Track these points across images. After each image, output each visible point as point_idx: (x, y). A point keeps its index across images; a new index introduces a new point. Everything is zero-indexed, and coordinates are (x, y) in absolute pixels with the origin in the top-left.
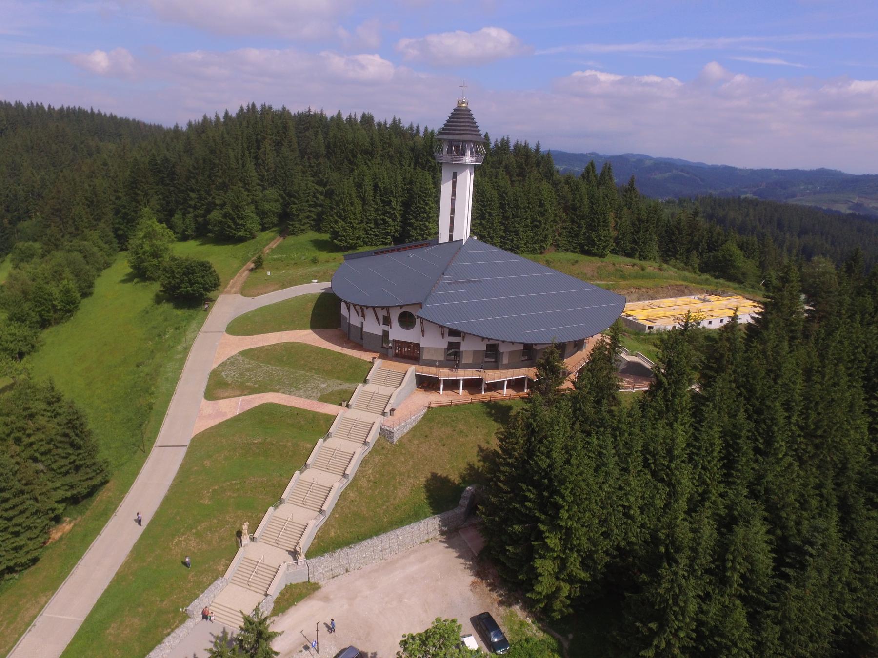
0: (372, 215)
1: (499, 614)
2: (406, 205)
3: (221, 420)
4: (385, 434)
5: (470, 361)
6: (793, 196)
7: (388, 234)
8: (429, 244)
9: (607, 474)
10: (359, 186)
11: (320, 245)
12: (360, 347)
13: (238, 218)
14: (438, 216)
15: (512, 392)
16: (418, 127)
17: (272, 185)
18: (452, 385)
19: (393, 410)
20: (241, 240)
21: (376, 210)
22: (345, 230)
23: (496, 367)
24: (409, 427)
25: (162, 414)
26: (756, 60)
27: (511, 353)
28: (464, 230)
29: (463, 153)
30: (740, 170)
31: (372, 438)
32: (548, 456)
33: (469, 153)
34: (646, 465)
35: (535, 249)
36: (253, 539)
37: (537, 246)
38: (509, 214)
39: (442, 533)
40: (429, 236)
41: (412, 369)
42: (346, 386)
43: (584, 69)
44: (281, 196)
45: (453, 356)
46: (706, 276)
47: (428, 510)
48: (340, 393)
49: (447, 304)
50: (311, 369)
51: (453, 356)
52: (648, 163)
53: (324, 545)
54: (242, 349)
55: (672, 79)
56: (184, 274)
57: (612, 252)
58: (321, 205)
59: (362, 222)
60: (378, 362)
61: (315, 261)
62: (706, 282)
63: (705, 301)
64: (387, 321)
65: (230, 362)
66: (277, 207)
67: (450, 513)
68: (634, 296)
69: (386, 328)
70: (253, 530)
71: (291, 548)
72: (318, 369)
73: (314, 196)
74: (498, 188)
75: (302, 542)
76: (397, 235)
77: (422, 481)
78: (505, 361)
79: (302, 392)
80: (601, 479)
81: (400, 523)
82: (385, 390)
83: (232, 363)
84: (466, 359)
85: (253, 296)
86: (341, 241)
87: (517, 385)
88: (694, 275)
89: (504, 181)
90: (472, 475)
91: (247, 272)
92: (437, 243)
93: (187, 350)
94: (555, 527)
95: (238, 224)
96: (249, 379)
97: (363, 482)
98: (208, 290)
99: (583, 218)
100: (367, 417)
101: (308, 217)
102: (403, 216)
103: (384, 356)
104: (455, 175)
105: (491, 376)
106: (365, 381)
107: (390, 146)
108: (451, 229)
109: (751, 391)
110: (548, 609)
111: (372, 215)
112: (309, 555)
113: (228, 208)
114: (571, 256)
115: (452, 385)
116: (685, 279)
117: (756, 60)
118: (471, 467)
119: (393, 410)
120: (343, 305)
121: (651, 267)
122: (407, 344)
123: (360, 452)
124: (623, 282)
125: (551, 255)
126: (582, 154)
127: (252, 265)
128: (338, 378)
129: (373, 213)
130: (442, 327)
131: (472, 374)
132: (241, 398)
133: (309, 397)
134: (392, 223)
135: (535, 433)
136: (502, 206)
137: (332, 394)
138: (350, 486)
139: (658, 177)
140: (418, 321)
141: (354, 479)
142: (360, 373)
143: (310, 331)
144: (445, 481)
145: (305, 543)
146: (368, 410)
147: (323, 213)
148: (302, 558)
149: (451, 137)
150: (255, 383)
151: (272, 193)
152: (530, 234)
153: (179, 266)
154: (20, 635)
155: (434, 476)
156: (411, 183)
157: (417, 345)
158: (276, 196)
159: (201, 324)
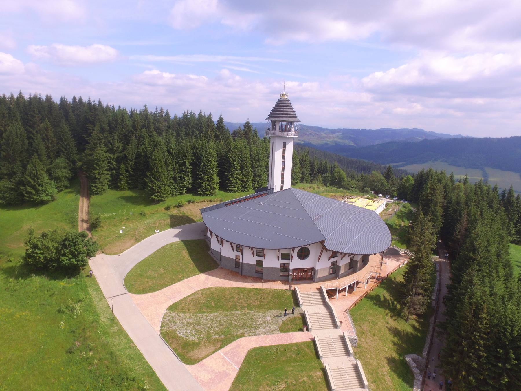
16: (113, 106)
20: (43, 203)
30: (235, 124)
40: (263, 189)
43: (150, 69)
50: (242, 308)
51: (335, 273)
54: (171, 303)
55: (203, 77)
58: (114, 169)
61: (142, 214)
76: (190, 186)
85: (118, 253)
86: (157, 196)
92: (273, 193)
93: (113, 319)
95: (39, 190)
122: (303, 270)
128: (270, 309)
132: (221, 352)
134: (187, 178)
151: (61, 161)
158: (63, 165)
159: (98, 290)
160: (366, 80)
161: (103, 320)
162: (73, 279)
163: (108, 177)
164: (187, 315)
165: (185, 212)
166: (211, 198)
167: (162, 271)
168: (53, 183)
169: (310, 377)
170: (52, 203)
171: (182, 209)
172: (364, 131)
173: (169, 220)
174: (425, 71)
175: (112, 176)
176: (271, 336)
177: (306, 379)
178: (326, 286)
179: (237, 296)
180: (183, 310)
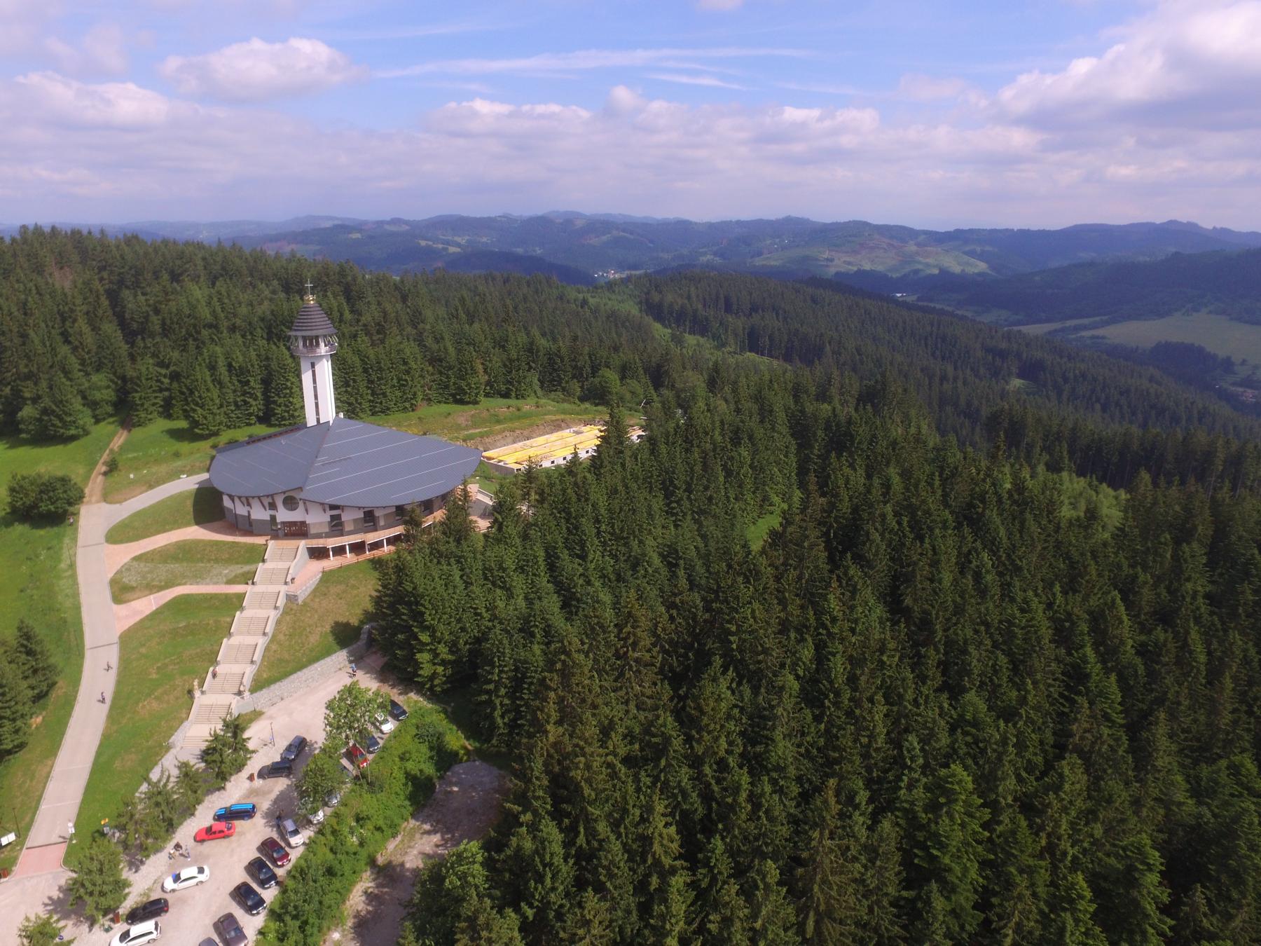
0: (231, 397)
1: (400, 700)
2: (266, 382)
3: (138, 619)
4: (291, 598)
5: (352, 528)
6: (760, 254)
7: (251, 414)
8: (298, 429)
9: (455, 587)
10: (212, 368)
11: (177, 435)
12: (249, 533)
13: (66, 414)
14: (301, 389)
15: (392, 548)
17: (98, 369)
18: (340, 551)
20: (73, 438)
21: (235, 391)
22: (205, 418)
23: (375, 529)
24: (309, 590)
26: (684, 79)
27: (386, 516)
28: (329, 411)
29: (318, 345)
31: (281, 602)
32: (412, 582)
33: (322, 345)
34: (486, 578)
35: (405, 408)
36: (203, 693)
37: (407, 405)
38: (374, 377)
41: (303, 544)
42: (246, 568)
44: (112, 381)
45: (337, 526)
46: (587, 405)
48: (243, 574)
49: (329, 481)
50: (209, 561)
51: (337, 526)
52: (580, 223)
53: (259, 685)
54: (133, 555)
56: (41, 492)
57: (487, 395)
58: (167, 389)
59: (221, 406)
60: (271, 543)
61: (177, 455)
62: (586, 411)
63: (578, 433)
64: (273, 506)
65: (126, 568)
66: (108, 394)
68: (510, 440)
69: (272, 512)
70: (201, 685)
71: (236, 691)
74: (358, 352)
75: (245, 681)
76: (261, 414)
77: (328, 628)
78: (382, 523)
80: (451, 591)
81: (317, 659)
82: (282, 565)
83: (128, 570)
84: (348, 528)
85: (120, 502)
87: (390, 541)
88: (573, 406)
89: (363, 342)
90: (369, 617)
91: (100, 478)
93: (72, 566)
94: (425, 628)
96: (153, 580)
97: (281, 637)
98: (70, 504)
99: (450, 368)
100: (273, 588)
101: (154, 405)
102: (264, 394)
103: (275, 537)
104: (313, 365)
105: (371, 538)
106: (264, 561)
107: (235, 315)
108: (318, 413)
109: (569, 513)
110: (431, 689)
111: (231, 397)
112: (252, 691)
113: (46, 402)
114: (444, 408)
115: (340, 551)
116: (564, 412)
117: (684, 79)
120: (225, 498)
121: (527, 406)
122: (294, 523)
123: (273, 615)
124: (498, 427)
125: (424, 410)
126: (489, 218)
127: (104, 469)
128: (237, 563)
129: (231, 395)
130: (322, 504)
133: (216, 583)
135: (400, 569)
136: (365, 371)
137: (236, 577)
138: (272, 641)
139: (594, 241)
140: (301, 503)
142: (258, 555)
143: (196, 527)
144: (347, 625)
145: (247, 681)
146: (272, 583)
147: (171, 398)
148: (247, 694)
149: (304, 333)
151: (99, 379)
152: (398, 394)
153: (32, 484)
154: (45, 784)
155: (337, 623)
156: (267, 359)
157: (303, 523)
158: (104, 383)
159: (75, 539)
160: (1007, 94)
163: (158, 401)
168: (88, 412)
172: (1025, 235)
174: (1180, 58)
175: (164, 400)
178: (318, 543)
180: (146, 561)
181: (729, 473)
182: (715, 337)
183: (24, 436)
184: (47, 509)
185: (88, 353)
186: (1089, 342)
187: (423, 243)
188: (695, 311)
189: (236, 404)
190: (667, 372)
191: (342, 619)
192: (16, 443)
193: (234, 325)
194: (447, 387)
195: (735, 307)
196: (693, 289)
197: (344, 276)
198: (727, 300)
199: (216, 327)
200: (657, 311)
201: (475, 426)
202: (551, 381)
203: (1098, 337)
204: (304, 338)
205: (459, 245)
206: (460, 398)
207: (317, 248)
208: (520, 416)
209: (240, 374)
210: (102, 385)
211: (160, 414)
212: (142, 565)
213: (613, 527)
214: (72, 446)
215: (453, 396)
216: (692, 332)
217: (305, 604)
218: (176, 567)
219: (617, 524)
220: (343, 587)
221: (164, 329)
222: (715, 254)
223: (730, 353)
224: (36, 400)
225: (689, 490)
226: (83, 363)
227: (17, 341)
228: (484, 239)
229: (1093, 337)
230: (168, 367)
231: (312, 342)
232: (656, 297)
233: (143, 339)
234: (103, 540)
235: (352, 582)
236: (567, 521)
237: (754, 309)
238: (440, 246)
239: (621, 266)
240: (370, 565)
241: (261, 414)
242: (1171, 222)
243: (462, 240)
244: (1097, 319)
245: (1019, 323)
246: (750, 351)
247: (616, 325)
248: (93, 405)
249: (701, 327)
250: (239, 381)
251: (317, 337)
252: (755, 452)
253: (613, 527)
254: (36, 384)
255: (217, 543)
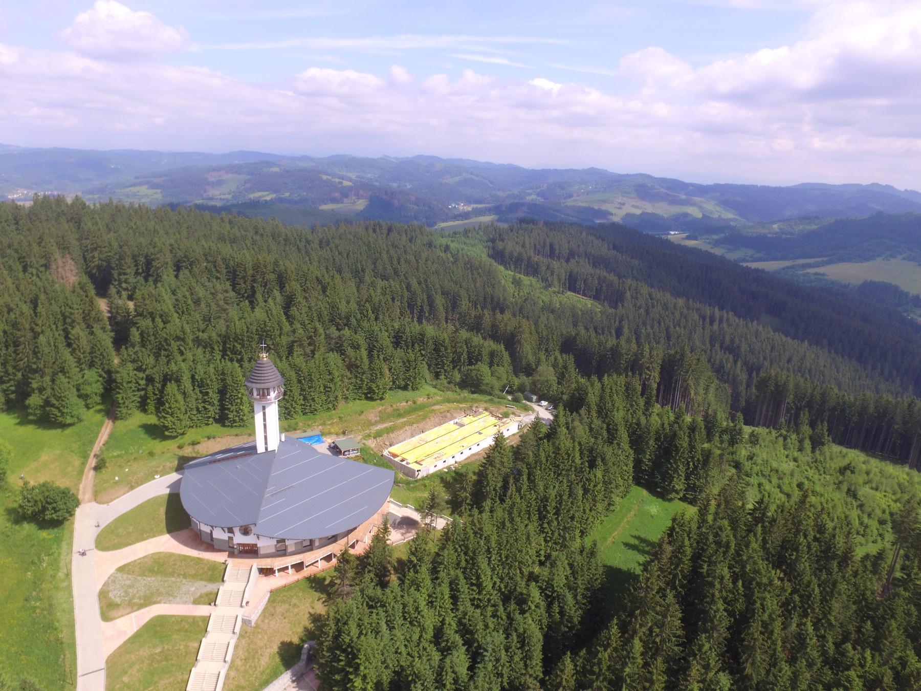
2: (222, 392)
4: (245, 622)
6: (571, 196)
7: (209, 417)
17: (91, 365)
19: (247, 603)
21: (197, 399)
25: (73, 646)
34: (405, 619)
35: (329, 408)
37: (330, 406)
39: (293, 682)
41: (256, 563)
44: (100, 376)
47: (282, 668)
48: (208, 594)
50: (179, 575)
51: (282, 552)
60: (231, 562)
61: (151, 454)
62: (464, 400)
64: (231, 530)
67: (296, 667)
69: (231, 535)
72: (185, 574)
73: (137, 383)
76: (217, 417)
77: (275, 649)
79: (178, 599)
83: (114, 582)
85: (107, 502)
91: (92, 473)
93: (68, 575)
96: (134, 596)
102: (220, 401)
103: (232, 555)
104: (264, 408)
108: (266, 443)
109: (467, 547)
116: (449, 401)
118: (306, 629)
119: (247, 603)
128: (202, 579)
129: (194, 403)
131: (296, 559)
132: (133, 615)
136: (299, 382)
137: (201, 596)
138: (230, 668)
141: (232, 661)
142: (218, 574)
143: (167, 537)
149: (259, 386)
150: (140, 598)
151: (92, 375)
155: (283, 643)
161: (61, 575)
162: (56, 530)
164: (130, 576)
165: (200, 451)
166: (238, 431)
167: (131, 529)
168: (81, 403)
169: (186, 646)
170: (78, 425)
171: (197, 447)
173: (176, 462)
175: (141, 397)
176: (184, 606)
177: (182, 647)
178: (266, 563)
179: (179, 563)
181: (586, 491)
182: (544, 280)
183: (31, 417)
184: (48, 513)
185: (84, 353)
186: (813, 278)
187: (325, 177)
188: (529, 258)
189: (198, 409)
190: (519, 342)
191: (287, 639)
192: (23, 422)
193: (197, 337)
194: (360, 388)
195: (557, 252)
196: (527, 238)
197: (278, 266)
198: (551, 246)
199: (183, 340)
200: (499, 256)
201: (382, 420)
202: (436, 365)
203: (819, 274)
204: (258, 390)
205: (350, 180)
206: (370, 396)
207: (248, 177)
208: (416, 408)
209: (200, 384)
210: (93, 381)
211: (138, 408)
212: (125, 576)
213: (500, 556)
214: (68, 431)
215: (365, 394)
216: (527, 274)
217: (257, 626)
218: (153, 581)
219: (504, 553)
220: (286, 606)
221: (142, 340)
222: (538, 195)
223: (554, 292)
224: (41, 390)
225: (557, 513)
226: (79, 361)
227: (29, 335)
228: (369, 176)
229: (816, 274)
230: (144, 371)
231: (264, 394)
232: (500, 245)
233: (126, 348)
234: (93, 546)
235: (294, 601)
236: (466, 554)
237: (572, 254)
238: (337, 180)
239: (469, 201)
240: (308, 584)
241: (217, 417)
242: (873, 184)
243: (353, 175)
244: (820, 259)
245: (760, 260)
246: (570, 290)
247: (472, 271)
248: (83, 397)
249: (532, 270)
250: (201, 392)
251: (268, 389)
252: (606, 471)
253: (500, 556)
254: (42, 377)
255: (185, 558)
